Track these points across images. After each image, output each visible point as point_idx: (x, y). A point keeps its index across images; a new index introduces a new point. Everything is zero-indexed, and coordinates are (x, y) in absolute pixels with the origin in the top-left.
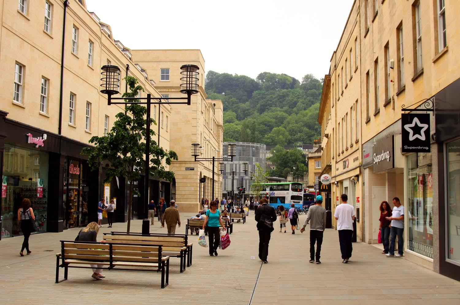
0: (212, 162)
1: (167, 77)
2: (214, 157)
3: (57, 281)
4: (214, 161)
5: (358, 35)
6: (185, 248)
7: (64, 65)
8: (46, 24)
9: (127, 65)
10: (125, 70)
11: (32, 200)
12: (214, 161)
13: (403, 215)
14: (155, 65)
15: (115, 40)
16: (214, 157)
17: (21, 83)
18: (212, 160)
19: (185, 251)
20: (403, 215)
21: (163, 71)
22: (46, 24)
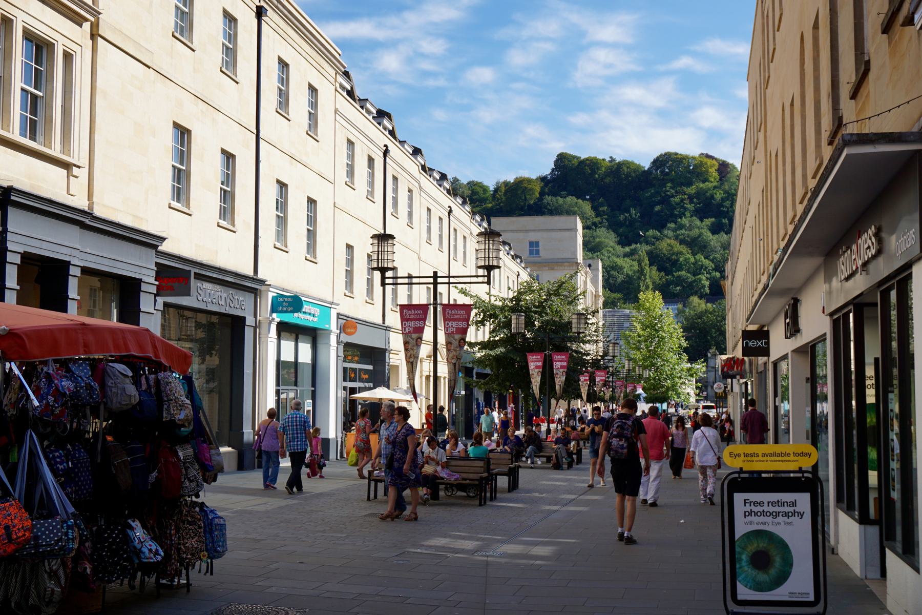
0: (431, 286)
1: (537, 252)
2: (435, 273)
3: (369, 499)
4: (435, 284)
5: (771, 64)
6: (485, 475)
7: (261, 135)
8: (179, 21)
9: (385, 146)
10: (382, 155)
11: (313, 389)
12: (435, 284)
13: (789, 411)
14: (521, 235)
15: (361, 98)
16: (435, 273)
17: (183, 165)
18: (431, 280)
19: (486, 479)
20: (789, 411)
21: (531, 244)
22: (179, 21)
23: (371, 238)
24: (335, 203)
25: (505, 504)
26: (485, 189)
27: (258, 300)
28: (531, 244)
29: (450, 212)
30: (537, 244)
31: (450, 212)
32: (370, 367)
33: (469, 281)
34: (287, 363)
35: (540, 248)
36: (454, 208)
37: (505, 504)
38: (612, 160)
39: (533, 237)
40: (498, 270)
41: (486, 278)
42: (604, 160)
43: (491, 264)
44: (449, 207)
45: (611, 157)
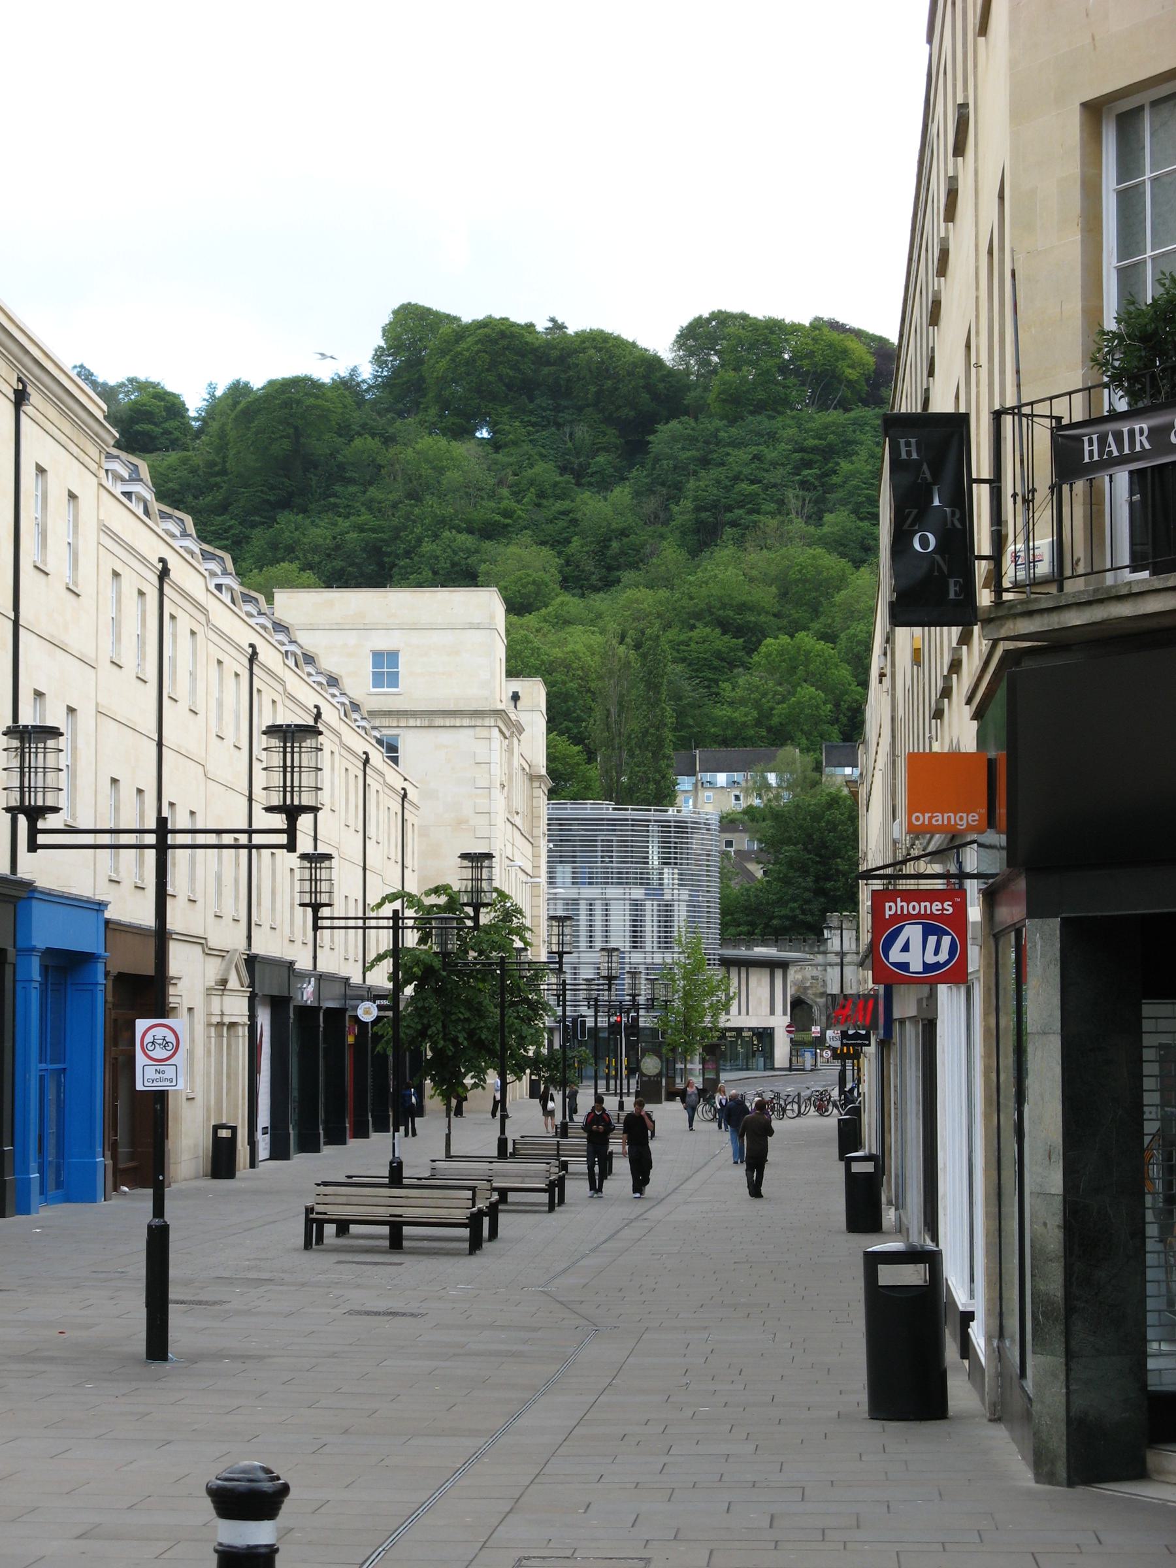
14: (352, 638)
21: (378, 656)
23: (4, 734)
24: (97, 704)
25: (1039, 644)
26: (172, 406)
27: (213, 1102)
28: (378, 656)
29: (164, 574)
30: (392, 657)
31: (164, 574)
32: (1173, 1073)
33: (92, 842)
34: (1162, 1097)
35: (402, 669)
36: (174, 563)
37: (1039, 644)
38: (557, 326)
39: (383, 642)
40: (311, 816)
41: (391, 921)
42: (530, 326)
43: (296, 802)
44: (162, 560)
45: (553, 320)
